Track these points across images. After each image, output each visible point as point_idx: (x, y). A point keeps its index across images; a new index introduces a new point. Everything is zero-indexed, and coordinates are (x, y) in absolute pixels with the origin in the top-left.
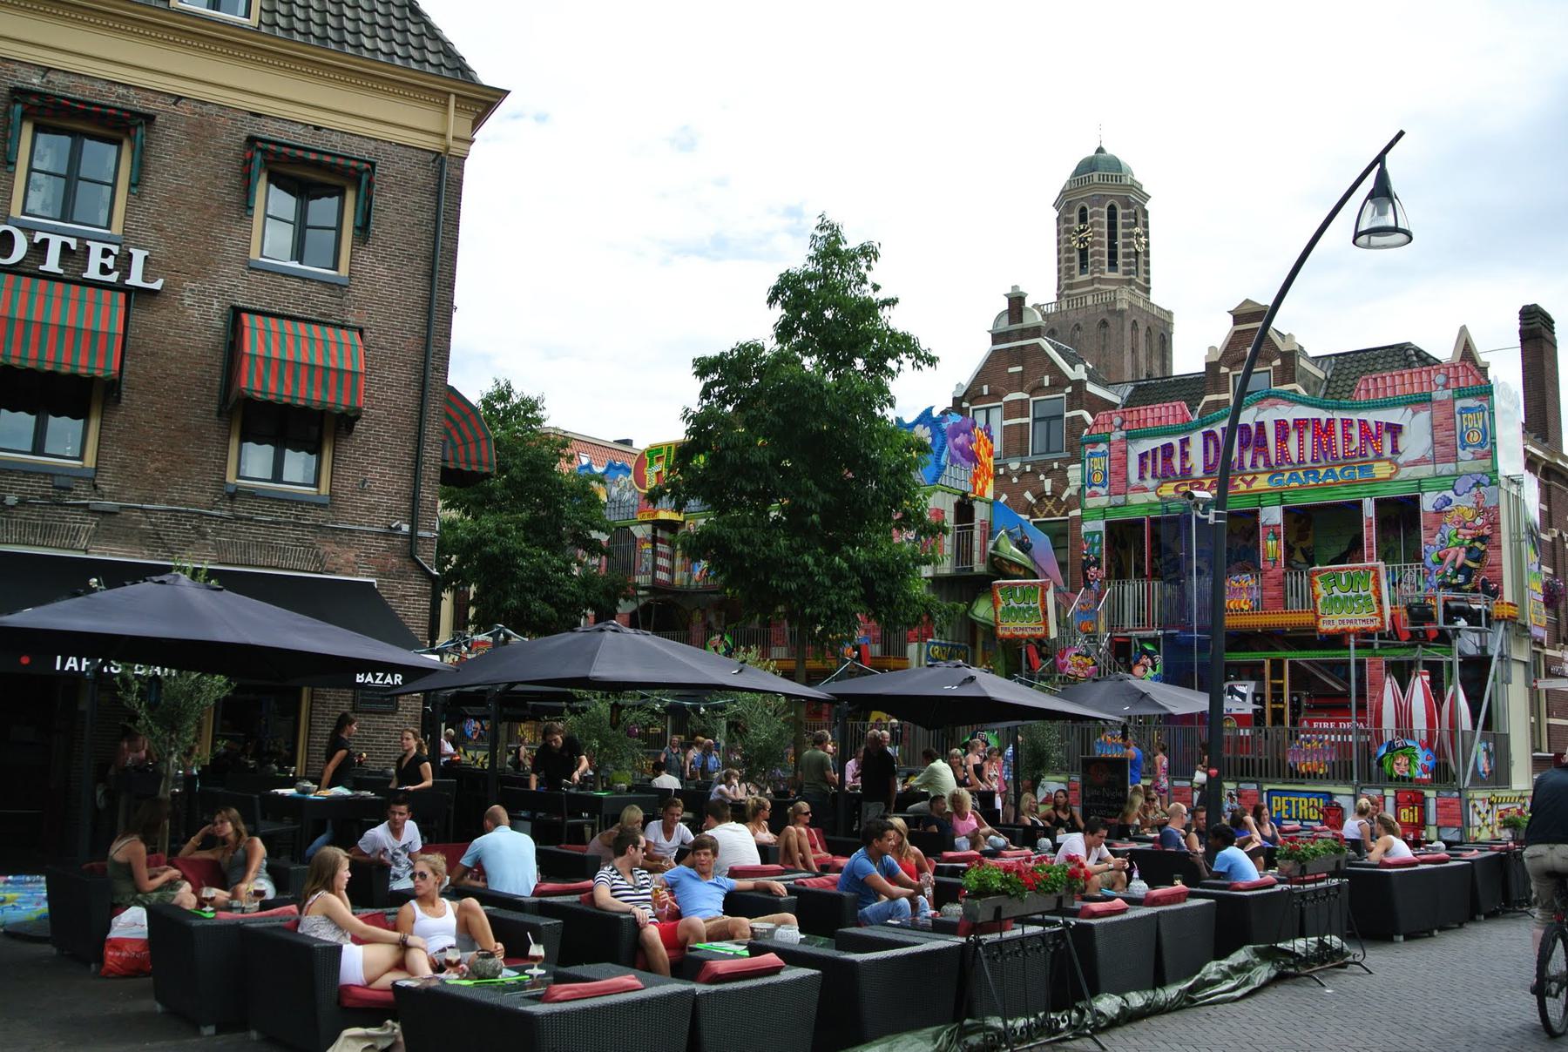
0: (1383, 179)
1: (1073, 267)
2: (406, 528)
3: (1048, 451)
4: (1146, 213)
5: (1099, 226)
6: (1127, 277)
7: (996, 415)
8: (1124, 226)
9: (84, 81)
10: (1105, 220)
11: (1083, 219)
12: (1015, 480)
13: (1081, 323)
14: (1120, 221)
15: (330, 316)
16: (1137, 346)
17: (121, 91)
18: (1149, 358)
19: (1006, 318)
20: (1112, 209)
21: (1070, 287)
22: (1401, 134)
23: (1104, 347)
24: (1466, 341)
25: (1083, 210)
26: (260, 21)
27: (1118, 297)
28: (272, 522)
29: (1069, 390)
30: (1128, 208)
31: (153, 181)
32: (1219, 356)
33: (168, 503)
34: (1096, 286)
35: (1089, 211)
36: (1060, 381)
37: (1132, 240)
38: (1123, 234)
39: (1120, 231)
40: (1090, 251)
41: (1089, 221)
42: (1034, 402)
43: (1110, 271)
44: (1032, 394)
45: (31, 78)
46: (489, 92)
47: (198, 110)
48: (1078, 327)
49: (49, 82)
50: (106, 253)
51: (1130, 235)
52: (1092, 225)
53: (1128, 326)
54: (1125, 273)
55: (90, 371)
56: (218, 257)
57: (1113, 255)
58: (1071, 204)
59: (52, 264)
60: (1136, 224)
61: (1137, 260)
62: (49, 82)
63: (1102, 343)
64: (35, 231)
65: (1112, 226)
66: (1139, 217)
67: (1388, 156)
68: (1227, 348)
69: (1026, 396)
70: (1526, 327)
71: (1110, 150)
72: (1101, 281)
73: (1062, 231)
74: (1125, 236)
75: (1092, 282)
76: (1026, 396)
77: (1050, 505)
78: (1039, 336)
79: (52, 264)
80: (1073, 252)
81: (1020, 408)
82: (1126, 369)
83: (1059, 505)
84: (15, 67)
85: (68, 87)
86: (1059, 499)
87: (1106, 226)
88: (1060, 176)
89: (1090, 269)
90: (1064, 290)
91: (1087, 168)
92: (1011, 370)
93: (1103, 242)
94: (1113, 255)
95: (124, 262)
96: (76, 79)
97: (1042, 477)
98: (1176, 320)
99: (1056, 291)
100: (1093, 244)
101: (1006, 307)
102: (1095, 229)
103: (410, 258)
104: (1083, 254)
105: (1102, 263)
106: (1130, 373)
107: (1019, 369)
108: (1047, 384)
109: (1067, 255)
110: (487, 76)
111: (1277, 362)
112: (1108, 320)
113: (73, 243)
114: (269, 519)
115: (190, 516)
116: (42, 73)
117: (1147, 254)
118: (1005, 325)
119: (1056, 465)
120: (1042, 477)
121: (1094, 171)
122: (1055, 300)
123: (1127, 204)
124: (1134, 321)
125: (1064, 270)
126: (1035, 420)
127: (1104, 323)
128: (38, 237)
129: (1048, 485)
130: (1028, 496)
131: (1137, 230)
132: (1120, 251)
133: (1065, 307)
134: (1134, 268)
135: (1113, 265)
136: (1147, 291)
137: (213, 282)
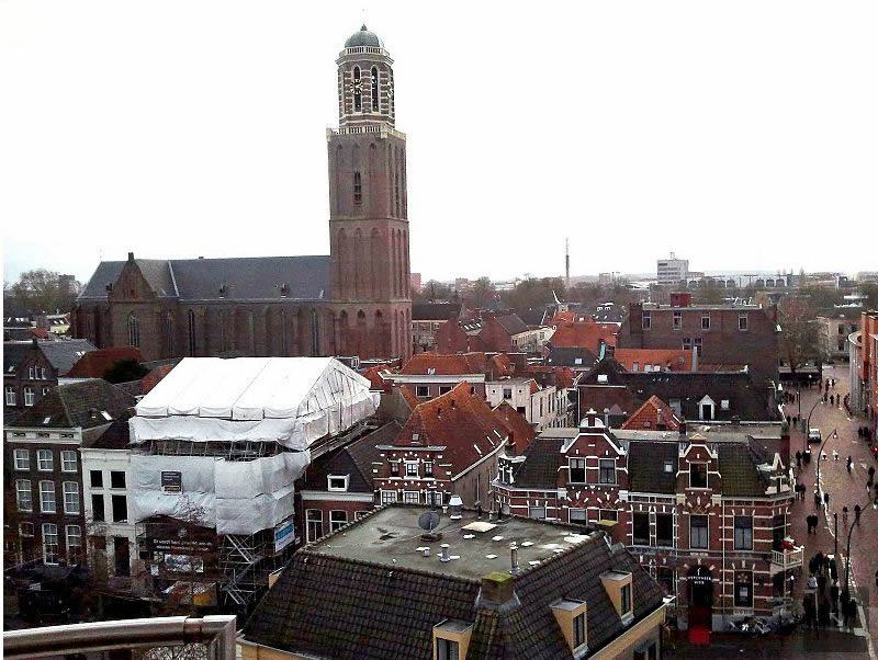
11: (357, 75)
52: (364, 81)
71: (371, 29)
75: (364, 117)
88: (338, 46)
94: (376, 102)
100: (364, 93)
104: (358, 98)
133: (347, 132)
136: (393, 122)
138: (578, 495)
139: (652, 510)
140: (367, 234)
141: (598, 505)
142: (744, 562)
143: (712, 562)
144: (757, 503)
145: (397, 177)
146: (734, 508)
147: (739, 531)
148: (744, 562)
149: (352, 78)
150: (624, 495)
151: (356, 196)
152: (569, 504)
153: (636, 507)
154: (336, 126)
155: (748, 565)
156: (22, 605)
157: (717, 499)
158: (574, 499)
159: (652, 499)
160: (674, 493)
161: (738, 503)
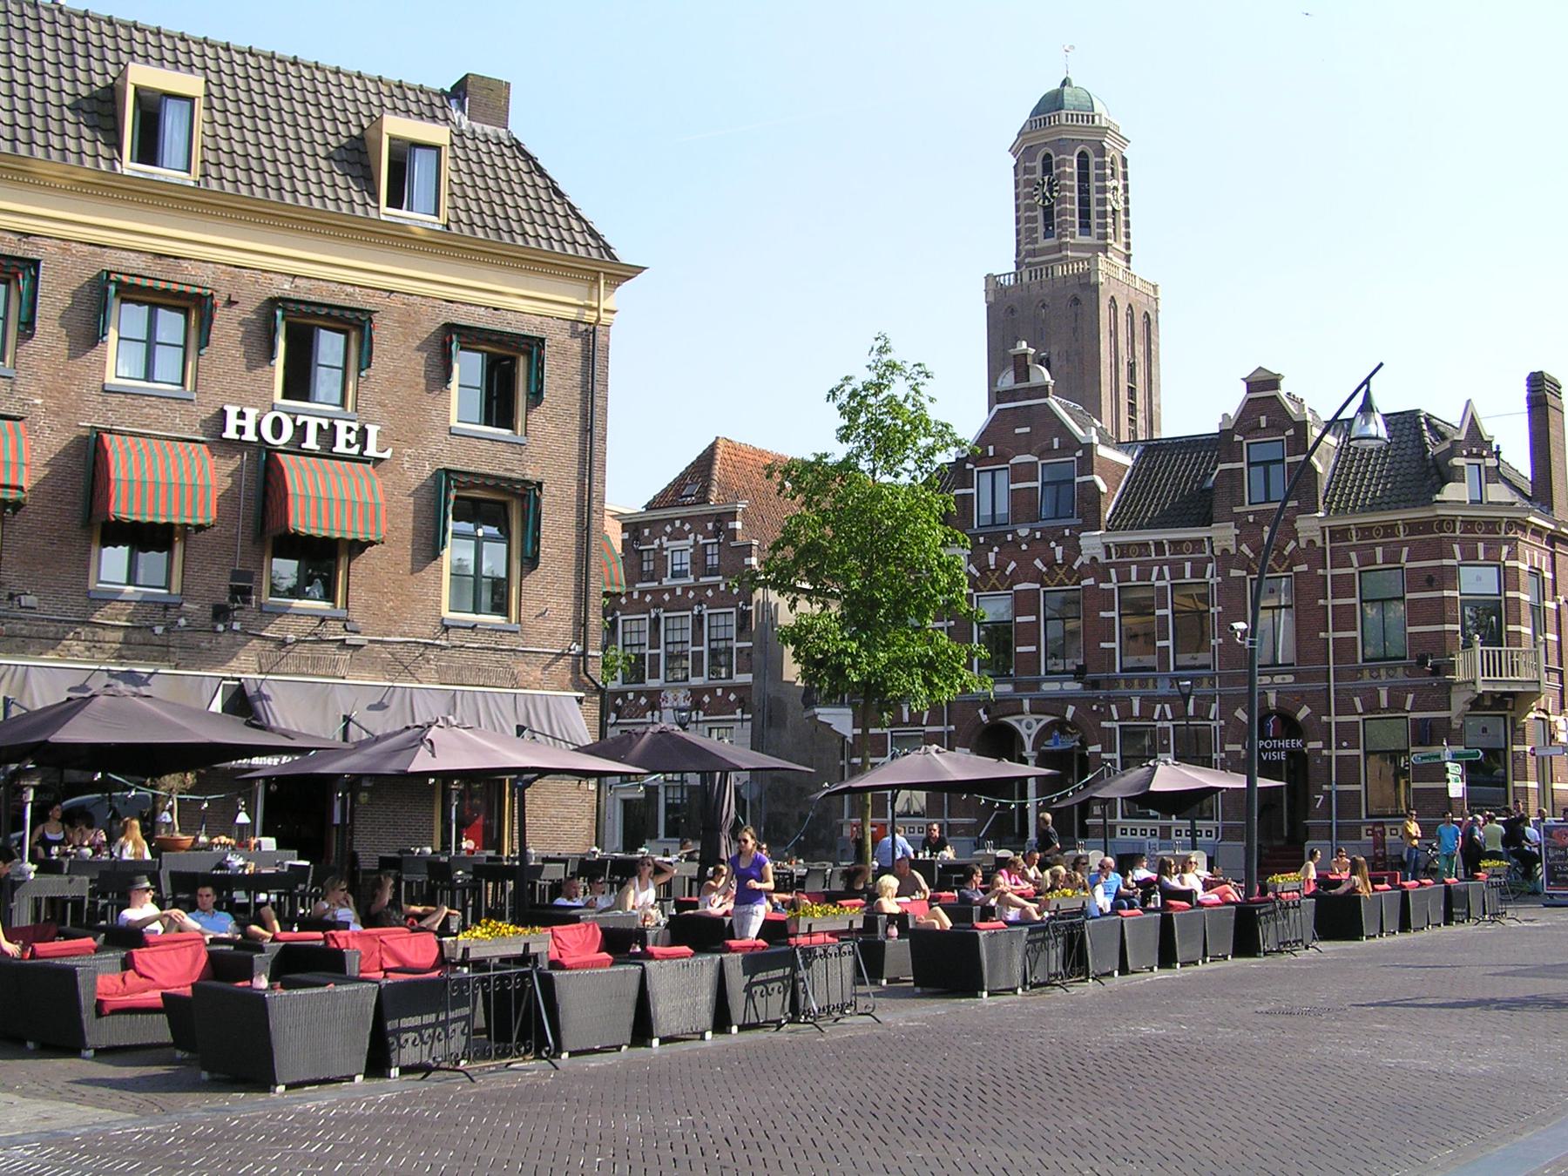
0: (1367, 395)
3: (1057, 517)
6: (1102, 242)
7: (1002, 478)
9: (321, 283)
11: (1047, 169)
12: (1024, 547)
13: (1048, 301)
15: (513, 471)
17: (349, 289)
22: (1381, 365)
23: (1075, 330)
24: (1472, 415)
25: (1048, 157)
26: (448, 220)
28: (478, 648)
29: (1079, 453)
32: (1233, 423)
33: (401, 636)
35: (1055, 159)
36: (1071, 442)
40: (1056, 209)
42: (1043, 465)
45: (283, 284)
46: (624, 268)
47: (406, 301)
49: (296, 287)
50: (349, 430)
55: (366, 536)
56: (427, 426)
59: (311, 443)
62: (296, 287)
63: (1073, 325)
64: (297, 414)
67: (1372, 380)
68: (1241, 416)
70: (1533, 394)
73: (1021, 183)
76: (1036, 459)
79: (311, 443)
81: (1027, 472)
83: (1070, 573)
84: (272, 276)
85: (310, 290)
90: (1026, 257)
91: (1052, 103)
95: (363, 435)
96: (316, 282)
97: (1053, 544)
104: (1048, 213)
107: (1027, 430)
110: (625, 255)
111: (1290, 432)
114: (476, 645)
116: (291, 279)
120: (1053, 544)
122: (1014, 270)
125: (1024, 234)
126: (1043, 484)
137: (424, 448)
138: (992, 557)
139: (1161, 577)
141: (1038, 577)
142: (1383, 694)
143: (1303, 698)
144: (1413, 527)
146: (1354, 548)
148: (1383, 694)
149: (1038, 175)
153: (1124, 576)
154: (1004, 262)
156: (892, 917)
158: (984, 568)
159: (1159, 545)
160: (1207, 521)
161: (1365, 531)
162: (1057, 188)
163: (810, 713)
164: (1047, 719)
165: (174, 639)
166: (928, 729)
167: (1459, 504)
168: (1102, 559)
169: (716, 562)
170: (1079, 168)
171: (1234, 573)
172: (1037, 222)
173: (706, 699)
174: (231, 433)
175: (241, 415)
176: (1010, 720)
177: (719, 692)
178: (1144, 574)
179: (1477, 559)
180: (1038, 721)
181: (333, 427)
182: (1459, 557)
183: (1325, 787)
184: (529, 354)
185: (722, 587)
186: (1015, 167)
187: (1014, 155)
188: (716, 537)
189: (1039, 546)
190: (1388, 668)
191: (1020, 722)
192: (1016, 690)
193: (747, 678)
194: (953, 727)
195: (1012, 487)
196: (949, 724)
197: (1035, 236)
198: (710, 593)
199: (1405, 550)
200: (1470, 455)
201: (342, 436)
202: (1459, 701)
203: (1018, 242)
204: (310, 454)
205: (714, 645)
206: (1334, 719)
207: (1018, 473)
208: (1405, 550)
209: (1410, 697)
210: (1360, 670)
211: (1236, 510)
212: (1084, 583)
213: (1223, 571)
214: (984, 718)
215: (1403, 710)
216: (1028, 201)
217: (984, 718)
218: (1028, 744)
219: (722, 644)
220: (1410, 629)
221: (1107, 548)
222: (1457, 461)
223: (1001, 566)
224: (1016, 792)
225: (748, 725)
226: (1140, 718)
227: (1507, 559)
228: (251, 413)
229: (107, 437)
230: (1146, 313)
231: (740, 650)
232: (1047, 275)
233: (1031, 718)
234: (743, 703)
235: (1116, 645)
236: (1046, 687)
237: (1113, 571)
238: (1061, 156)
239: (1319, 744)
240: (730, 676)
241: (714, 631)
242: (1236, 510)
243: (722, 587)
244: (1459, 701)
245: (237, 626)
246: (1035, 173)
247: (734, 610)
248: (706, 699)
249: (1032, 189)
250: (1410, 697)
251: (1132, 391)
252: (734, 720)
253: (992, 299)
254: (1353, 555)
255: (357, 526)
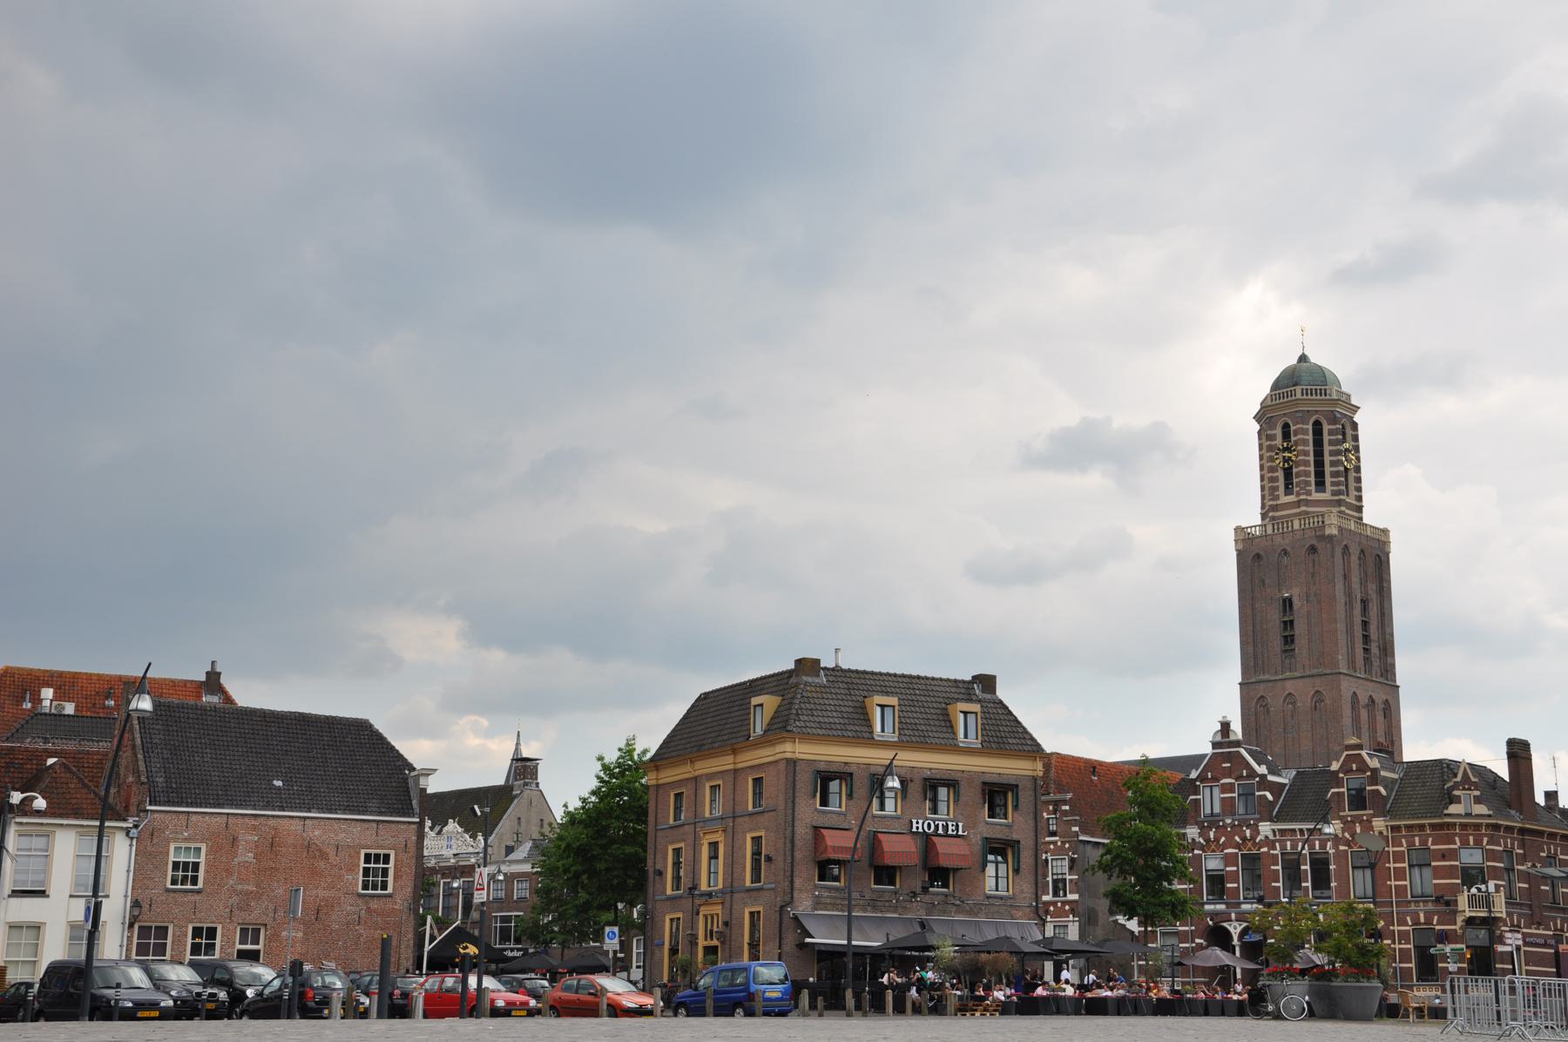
1: (1278, 487)
2: (1034, 904)
4: (1355, 426)
5: (1305, 455)
7: (1216, 791)
8: (1331, 443)
10: (1310, 437)
11: (1286, 435)
12: (1229, 829)
13: (1288, 549)
14: (1326, 438)
16: (1349, 571)
18: (1363, 582)
19: (1219, 734)
20: (1317, 424)
21: (1274, 508)
23: (1313, 575)
25: (1286, 426)
27: (1326, 523)
29: (1257, 779)
30: (1335, 424)
31: (963, 798)
34: (1303, 508)
35: (1293, 428)
37: (1340, 458)
38: (1330, 451)
39: (1327, 448)
40: (1295, 470)
41: (1293, 439)
43: (1316, 491)
44: (1236, 779)
48: (1285, 552)
50: (953, 825)
51: (1338, 453)
53: (1338, 551)
54: (1334, 493)
57: (1320, 474)
58: (1273, 420)
59: (940, 831)
60: (1344, 440)
61: (1347, 480)
63: (1311, 571)
65: (1318, 443)
66: (1348, 430)
69: (1233, 781)
71: (1315, 358)
72: (1307, 503)
74: (1332, 453)
75: (1298, 503)
76: (1233, 781)
77: (1250, 844)
78: (1239, 747)
79: (940, 831)
80: (1277, 471)
81: (1230, 788)
82: (1338, 597)
83: (1255, 844)
86: (1255, 841)
87: (1312, 453)
89: (1295, 489)
92: (1224, 765)
93: (1310, 472)
94: (1320, 474)
95: (957, 826)
97: (1244, 828)
98: (1393, 537)
99: (1259, 511)
101: (1220, 728)
102: (1299, 448)
103: (1029, 813)
104: (1288, 473)
105: (1308, 483)
106: (1343, 601)
107: (1229, 765)
108: (1245, 774)
109: (1270, 475)
111: (1369, 773)
112: (1317, 545)
113: (944, 823)
115: (978, 904)
117: (1358, 469)
118: (1219, 738)
119: (1252, 822)
120: (1244, 828)
121: (1296, 384)
122: (1259, 522)
123: (1333, 419)
124: (1346, 546)
125: (1268, 491)
126: (1239, 795)
127: (1313, 549)
128: (937, 823)
129: (1248, 833)
130: (1237, 838)
131: (1346, 445)
132: (1328, 469)
133: (1270, 531)
134: (1343, 488)
135: (1320, 484)
136: (1360, 509)
138: (1212, 835)
140: (1304, 703)
141: (1237, 846)
142: (1422, 915)
144: (1433, 827)
145: (1364, 603)
147: (1416, 871)
148: (1422, 915)
150: (1265, 828)
151: (1286, 637)
152: (1202, 848)
153: (1283, 847)
154: (1251, 516)
155: (1429, 921)
157: (1379, 824)
158: (1208, 840)
159: (1301, 831)
161: (1409, 827)
162: (1295, 453)
163: (1114, 918)
164: (1245, 924)
165: (899, 904)
166: (1180, 928)
167: (1458, 816)
168: (1271, 837)
169: (1055, 829)
170: (1314, 446)
171: (1342, 848)
172: (1278, 481)
173: (1052, 908)
174: (914, 830)
175: (917, 823)
176: (1225, 924)
177: (1059, 904)
178: (1294, 846)
179: (1469, 844)
180: (1240, 925)
181: (947, 825)
182: (1459, 844)
183: (1394, 965)
184: (1012, 791)
185: (1059, 844)
186: (1259, 432)
187: (1258, 421)
188: (1055, 814)
189: (1237, 828)
190: (1424, 902)
191: (1230, 925)
192: (1227, 908)
193: (1075, 897)
194: (1193, 928)
195: (1222, 796)
196: (1192, 926)
197: (1276, 493)
198: (1052, 847)
199: (1430, 839)
200: (1464, 789)
201: (950, 828)
202: (1460, 920)
203: (1263, 497)
204: (940, 835)
205: (1055, 877)
206: (1396, 928)
207: (1230, 788)
208: (1430, 839)
209: (1436, 918)
210: (1410, 902)
211: (1341, 814)
212: (1262, 850)
213: (1335, 846)
214: (1211, 923)
215: (1433, 925)
216: (1269, 464)
217: (1211, 923)
218: (1235, 938)
219: (1060, 877)
220: (1435, 881)
221: (1274, 831)
222: (1456, 793)
223: (1217, 840)
224: (1415, 978)
225: (1077, 924)
226: (1425, 924)
227: (1487, 844)
228: (921, 822)
229: (879, 835)
230: (1378, 556)
231: (1071, 880)
232: (1288, 527)
233: (1236, 924)
234: (1073, 911)
235: (1280, 884)
236: (1244, 907)
237: (1277, 844)
238: (1298, 426)
239: (1389, 942)
240: (1065, 895)
241: (1055, 868)
242: (1341, 814)
243: (1059, 844)
244: (1460, 920)
245: (919, 899)
246: (1275, 440)
247: (1066, 857)
248: (1052, 908)
249: (1274, 454)
250: (1436, 918)
251: (1365, 624)
252: (1069, 921)
253: (1241, 547)
254: (1403, 841)
255: (957, 863)
